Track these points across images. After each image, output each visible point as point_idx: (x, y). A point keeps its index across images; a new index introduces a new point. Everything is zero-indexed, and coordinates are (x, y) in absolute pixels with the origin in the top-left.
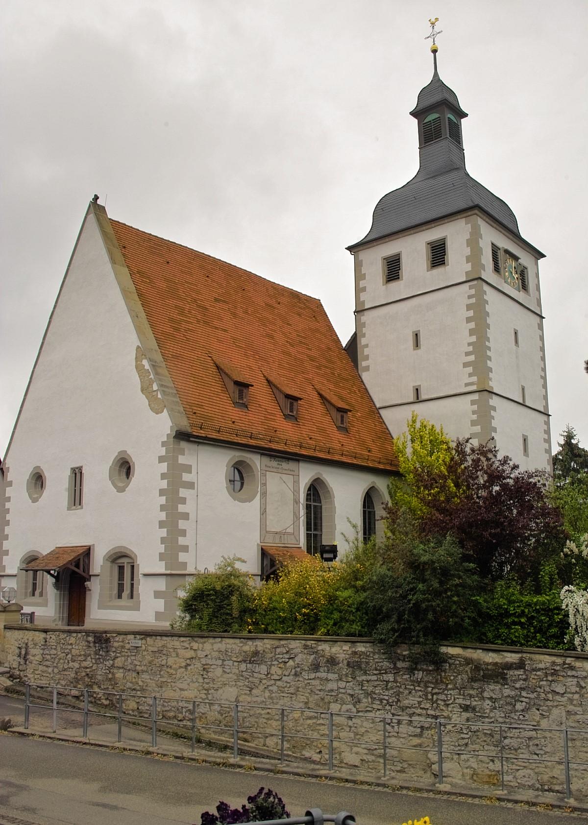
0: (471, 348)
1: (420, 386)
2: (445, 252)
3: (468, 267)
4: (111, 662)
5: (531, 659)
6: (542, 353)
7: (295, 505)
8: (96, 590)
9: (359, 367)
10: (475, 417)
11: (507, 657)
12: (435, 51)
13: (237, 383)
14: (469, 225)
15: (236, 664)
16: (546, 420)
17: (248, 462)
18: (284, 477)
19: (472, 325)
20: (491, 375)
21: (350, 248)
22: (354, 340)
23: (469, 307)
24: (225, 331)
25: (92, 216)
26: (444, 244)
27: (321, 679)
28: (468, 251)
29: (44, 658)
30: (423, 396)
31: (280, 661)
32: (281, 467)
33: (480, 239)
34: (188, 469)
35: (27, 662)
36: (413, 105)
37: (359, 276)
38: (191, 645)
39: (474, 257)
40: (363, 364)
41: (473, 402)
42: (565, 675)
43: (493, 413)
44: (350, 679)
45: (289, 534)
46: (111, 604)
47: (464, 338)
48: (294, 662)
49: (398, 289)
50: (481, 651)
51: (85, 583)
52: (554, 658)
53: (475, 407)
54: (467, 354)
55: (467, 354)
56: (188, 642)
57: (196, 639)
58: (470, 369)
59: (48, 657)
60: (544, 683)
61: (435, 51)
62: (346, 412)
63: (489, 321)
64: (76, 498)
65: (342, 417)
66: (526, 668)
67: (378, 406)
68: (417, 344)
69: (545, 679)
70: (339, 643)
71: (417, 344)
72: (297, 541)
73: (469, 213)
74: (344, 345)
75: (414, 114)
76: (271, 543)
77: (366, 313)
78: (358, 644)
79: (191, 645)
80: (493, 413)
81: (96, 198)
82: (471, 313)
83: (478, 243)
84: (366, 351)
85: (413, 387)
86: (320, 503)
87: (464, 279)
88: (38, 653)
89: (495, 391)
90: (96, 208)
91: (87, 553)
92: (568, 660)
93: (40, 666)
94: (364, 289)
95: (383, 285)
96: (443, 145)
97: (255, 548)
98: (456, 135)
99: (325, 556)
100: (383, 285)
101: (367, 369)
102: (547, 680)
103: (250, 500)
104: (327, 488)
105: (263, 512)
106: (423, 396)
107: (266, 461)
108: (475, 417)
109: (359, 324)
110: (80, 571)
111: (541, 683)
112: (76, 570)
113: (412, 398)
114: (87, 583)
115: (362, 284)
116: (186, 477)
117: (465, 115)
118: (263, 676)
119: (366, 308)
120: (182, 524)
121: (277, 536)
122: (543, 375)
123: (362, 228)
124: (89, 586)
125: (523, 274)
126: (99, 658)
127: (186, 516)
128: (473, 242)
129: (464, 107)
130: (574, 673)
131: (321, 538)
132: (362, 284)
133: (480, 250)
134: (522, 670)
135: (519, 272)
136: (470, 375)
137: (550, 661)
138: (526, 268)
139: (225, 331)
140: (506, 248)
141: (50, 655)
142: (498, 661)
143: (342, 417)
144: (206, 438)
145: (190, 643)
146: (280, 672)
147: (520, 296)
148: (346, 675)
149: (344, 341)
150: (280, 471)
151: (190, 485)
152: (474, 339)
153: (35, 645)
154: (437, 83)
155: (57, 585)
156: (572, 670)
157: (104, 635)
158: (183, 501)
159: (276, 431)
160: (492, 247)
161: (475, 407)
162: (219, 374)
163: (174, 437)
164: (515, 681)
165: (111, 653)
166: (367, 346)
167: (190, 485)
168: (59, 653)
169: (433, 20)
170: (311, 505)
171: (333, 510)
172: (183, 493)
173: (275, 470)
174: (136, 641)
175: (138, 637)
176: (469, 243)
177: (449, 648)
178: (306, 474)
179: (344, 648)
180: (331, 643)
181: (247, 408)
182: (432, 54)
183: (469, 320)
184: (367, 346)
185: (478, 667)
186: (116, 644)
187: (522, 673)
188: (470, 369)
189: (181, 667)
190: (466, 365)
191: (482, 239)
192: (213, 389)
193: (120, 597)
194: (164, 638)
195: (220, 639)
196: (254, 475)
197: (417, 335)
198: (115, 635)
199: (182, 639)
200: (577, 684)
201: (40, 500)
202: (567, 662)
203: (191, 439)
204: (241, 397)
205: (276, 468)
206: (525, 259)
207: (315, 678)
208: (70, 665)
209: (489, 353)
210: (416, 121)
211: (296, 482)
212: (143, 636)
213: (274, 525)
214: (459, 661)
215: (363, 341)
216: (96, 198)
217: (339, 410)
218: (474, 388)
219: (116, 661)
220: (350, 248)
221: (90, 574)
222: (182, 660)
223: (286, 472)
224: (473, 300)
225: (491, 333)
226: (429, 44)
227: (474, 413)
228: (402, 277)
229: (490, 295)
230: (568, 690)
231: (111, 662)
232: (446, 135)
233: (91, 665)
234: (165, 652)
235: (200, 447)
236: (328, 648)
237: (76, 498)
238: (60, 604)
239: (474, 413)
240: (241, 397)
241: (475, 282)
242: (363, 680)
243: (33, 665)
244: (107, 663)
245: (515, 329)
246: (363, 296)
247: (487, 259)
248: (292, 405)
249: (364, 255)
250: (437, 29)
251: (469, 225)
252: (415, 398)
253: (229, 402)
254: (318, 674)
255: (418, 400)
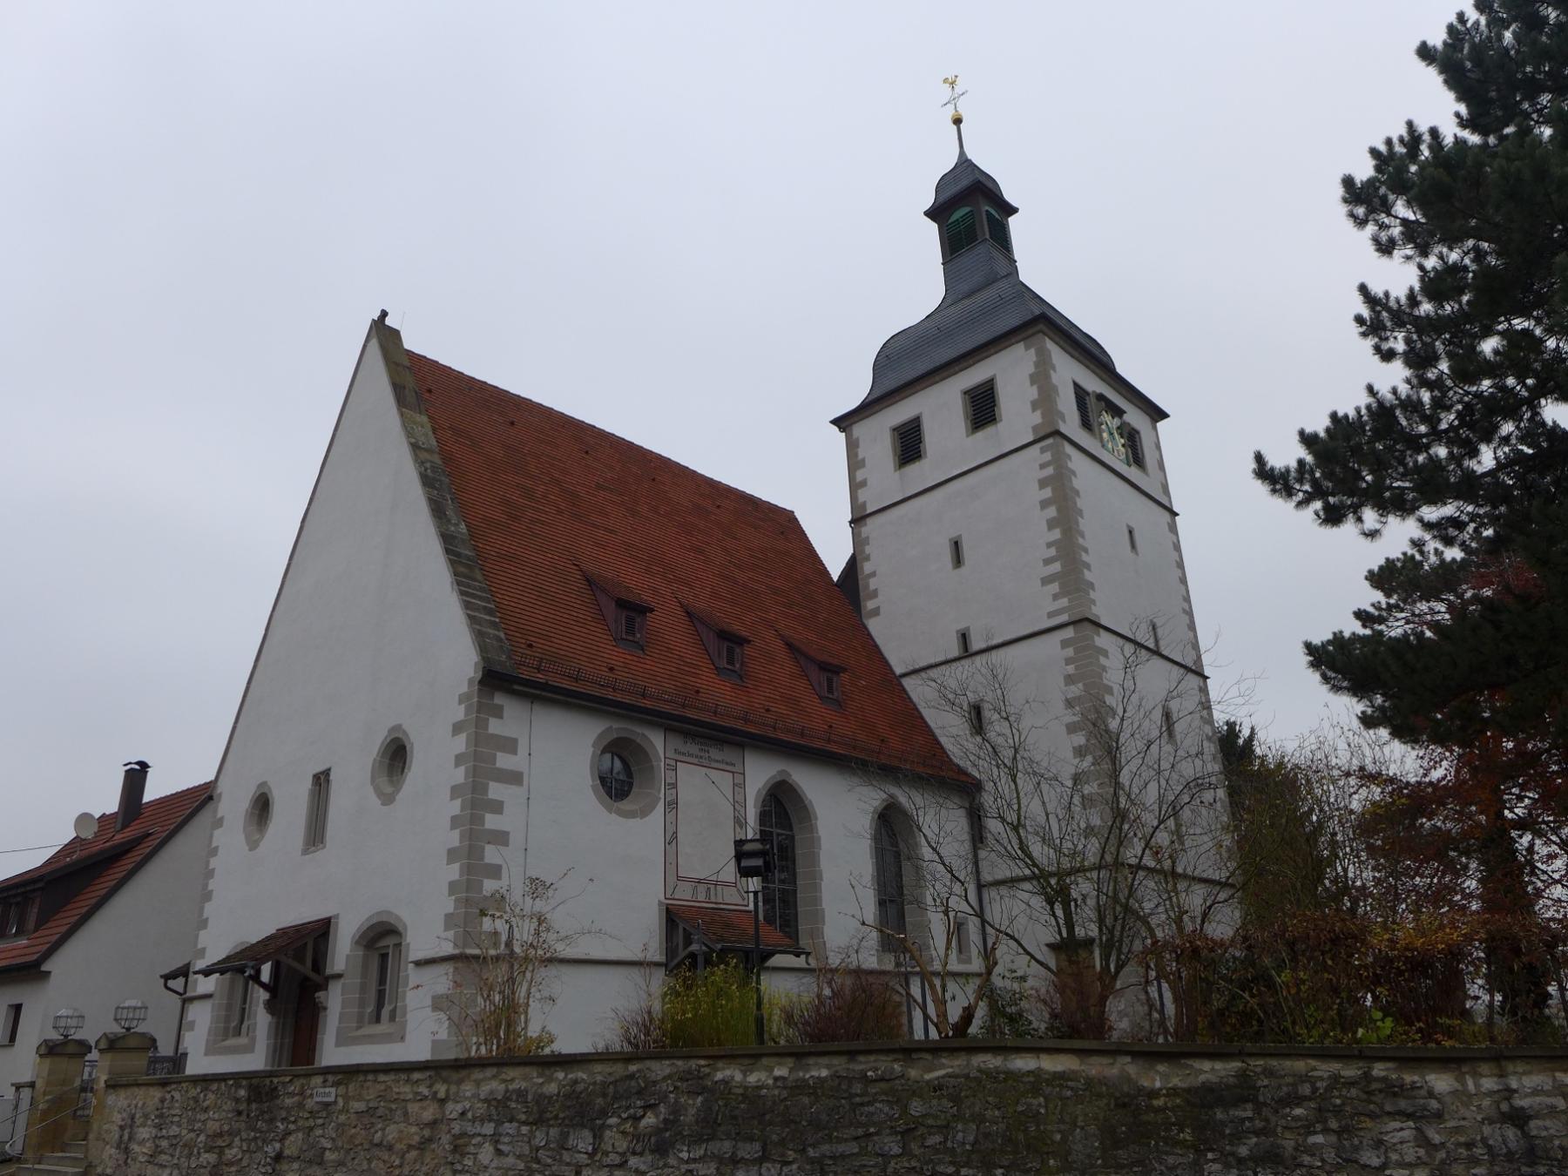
0: (1052, 552)
1: (968, 628)
2: (994, 401)
3: (1037, 418)
4: (278, 1145)
5: (1270, 1073)
6: (1180, 571)
7: (738, 829)
8: (335, 1001)
9: (863, 612)
10: (1071, 669)
11: (1202, 1072)
12: (958, 121)
13: (622, 604)
14: (1032, 351)
15: (525, 1129)
16: (1202, 684)
17: (638, 741)
18: (714, 774)
19: (1052, 512)
20: (1092, 595)
21: (836, 422)
22: (852, 566)
23: (1043, 483)
24: (611, 531)
25: (374, 343)
26: (992, 388)
27: (720, 1160)
28: (1033, 393)
29: (157, 1146)
30: (976, 644)
31: (624, 1115)
32: (707, 755)
33: (1052, 372)
34: (510, 746)
35: (129, 1161)
36: (929, 200)
37: (854, 463)
38: (434, 1089)
39: (1045, 399)
40: (870, 605)
41: (1065, 644)
42: (1377, 1111)
43: (1103, 660)
44: (791, 1155)
45: (726, 884)
46: (360, 1033)
47: (1039, 535)
48: (657, 1116)
49: (922, 473)
50: (1128, 1059)
51: (317, 995)
52: (1334, 1067)
53: (1070, 652)
54: (1047, 562)
55: (1047, 562)
56: (428, 1082)
57: (445, 1074)
58: (1055, 587)
59: (164, 1143)
60: (1319, 1139)
61: (958, 121)
62: (837, 673)
63: (1080, 503)
64: (316, 834)
65: (830, 682)
66: (1261, 1099)
67: (898, 670)
68: (958, 561)
69: (1319, 1127)
70: (765, 1061)
71: (958, 561)
72: (744, 900)
73: (1030, 331)
74: (835, 578)
75: (931, 214)
76: (684, 894)
77: (869, 521)
78: (811, 1061)
79: (434, 1089)
80: (1103, 660)
81: (384, 314)
82: (1047, 493)
83: (1048, 377)
84: (873, 584)
85: (957, 632)
86: (791, 830)
87: (1031, 438)
88: (147, 1136)
89: (1103, 622)
90: (383, 333)
91: (321, 931)
92: (1379, 1070)
93: (150, 1167)
94: (863, 484)
95: (895, 471)
96: (984, 249)
97: (655, 908)
98: (1002, 239)
99: (744, 863)
100: (895, 471)
101: (876, 612)
102: (1326, 1131)
103: (644, 813)
104: (802, 801)
105: (672, 839)
106: (976, 644)
107: (676, 742)
108: (1071, 669)
109: (858, 541)
110: (307, 969)
111: (1312, 1139)
112: (296, 965)
113: (955, 651)
114: (320, 995)
115: (860, 476)
116: (504, 761)
117: (1013, 210)
118: (583, 1158)
119: (868, 511)
120: (491, 854)
121: (702, 888)
122: (1187, 608)
123: (858, 389)
124: (322, 999)
125: (1132, 438)
126: (256, 1138)
127: (501, 838)
128: (1041, 376)
129: (1009, 196)
130: (1403, 1104)
131: (796, 897)
132: (860, 476)
133: (1055, 389)
134: (1249, 1106)
135: (1126, 435)
136: (1056, 597)
137: (1326, 1075)
138: (1138, 432)
139: (611, 531)
140: (1098, 391)
141: (168, 1138)
142: (1179, 1084)
143: (830, 682)
144: (545, 687)
145: (430, 1087)
146: (622, 1145)
147: (1133, 473)
148: (782, 1142)
149: (835, 569)
150: (705, 762)
151: (515, 778)
152: (1056, 534)
153: (146, 1116)
154: (964, 164)
155: (270, 1006)
156: (1395, 1095)
157: (267, 1081)
158: (497, 807)
159: (698, 692)
160: (1075, 389)
161: (1070, 652)
162: (590, 592)
163: (480, 682)
164: (1237, 1137)
165: (279, 1124)
166: (873, 574)
167: (515, 778)
168: (184, 1132)
169: (950, 77)
170: (771, 832)
171: (814, 842)
172: (496, 791)
173: (696, 761)
174: (327, 1090)
175: (331, 1078)
176: (1034, 379)
177: (1043, 1056)
178: (759, 773)
179: (778, 1072)
180: (746, 1061)
181: (643, 650)
182: (955, 127)
183: (1044, 504)
184: (873, 574)
185: (1129, 1101)
186: (288, 1101)
187: (1249, 1114)
188: (1055, 587)
189: (410, 1147)
190: (1046, 581)
191: (1055, 371)
192: (575, 614)
193: (378, 1020)
194: (382, 1078)
195: (494, 1070)
196: (652, 767)
197: (956, 543)
198: (288, 1079)
199: (416, 1076)
200: (1416, 1139)
201: (261, 844)
202: (1375, 1073)
203: (516, 687)
204: (630, 629)
205: (697, 757)
206: (1134, 417)
207: (705, 1155)
208: (201, 1159)
209: (1085, 557)
210: (932, 228)
211: (739, 786)
212: (340, 1077)
213: (694, 867)
214: (1072, 1089)
215: (867, 567)
216: (384, 314)
217: (824, 667)
218: (1064, 618)
219: (287, 1143)
220: (836, 422)
221: (329, 971)
222: (414, 1129)
223: (716, 765)
224: (1050, 471)
225: (1084, 524)
226: (949, 112)
227: (1068, 661)
228: (925, 453)
229: (1077, 461)
230: (1394, 1157)
231: (278, 1145)
232: (984, 234)
233: (239, 1157)
234: (380, 1112)
235: (537, 708)
236: (738, 1077)
237: (316, 834)
238: (276, 1043)
239: (1068, 661)
240: (630, 629)
241: (1050, 441)
242: (824, 1156)
243: (138, 1165)
244: (269, 1149)
245: (1128, 526)
246: (863, 495)
247: (1067, 403)
248: (730, 652)
249: (860, 429)
250: (958, 89)
251: (1032, 351)
252: (962, 651)
253: (605, 637)
254: (714, 1147)
255: (967, 651)
